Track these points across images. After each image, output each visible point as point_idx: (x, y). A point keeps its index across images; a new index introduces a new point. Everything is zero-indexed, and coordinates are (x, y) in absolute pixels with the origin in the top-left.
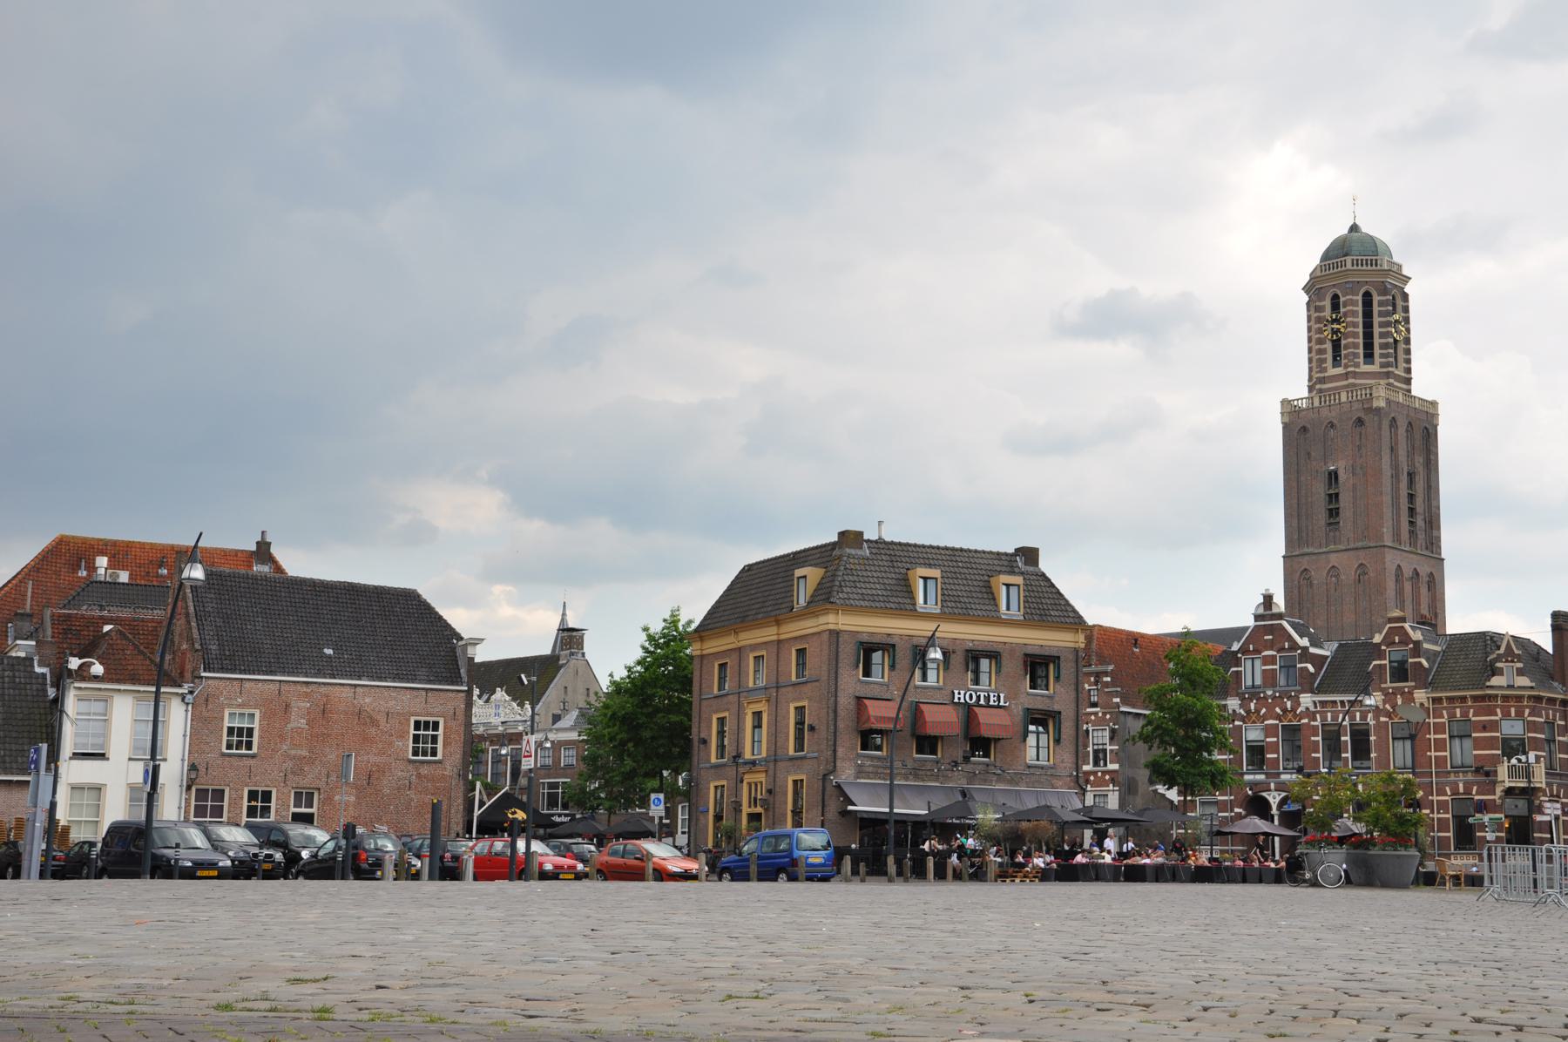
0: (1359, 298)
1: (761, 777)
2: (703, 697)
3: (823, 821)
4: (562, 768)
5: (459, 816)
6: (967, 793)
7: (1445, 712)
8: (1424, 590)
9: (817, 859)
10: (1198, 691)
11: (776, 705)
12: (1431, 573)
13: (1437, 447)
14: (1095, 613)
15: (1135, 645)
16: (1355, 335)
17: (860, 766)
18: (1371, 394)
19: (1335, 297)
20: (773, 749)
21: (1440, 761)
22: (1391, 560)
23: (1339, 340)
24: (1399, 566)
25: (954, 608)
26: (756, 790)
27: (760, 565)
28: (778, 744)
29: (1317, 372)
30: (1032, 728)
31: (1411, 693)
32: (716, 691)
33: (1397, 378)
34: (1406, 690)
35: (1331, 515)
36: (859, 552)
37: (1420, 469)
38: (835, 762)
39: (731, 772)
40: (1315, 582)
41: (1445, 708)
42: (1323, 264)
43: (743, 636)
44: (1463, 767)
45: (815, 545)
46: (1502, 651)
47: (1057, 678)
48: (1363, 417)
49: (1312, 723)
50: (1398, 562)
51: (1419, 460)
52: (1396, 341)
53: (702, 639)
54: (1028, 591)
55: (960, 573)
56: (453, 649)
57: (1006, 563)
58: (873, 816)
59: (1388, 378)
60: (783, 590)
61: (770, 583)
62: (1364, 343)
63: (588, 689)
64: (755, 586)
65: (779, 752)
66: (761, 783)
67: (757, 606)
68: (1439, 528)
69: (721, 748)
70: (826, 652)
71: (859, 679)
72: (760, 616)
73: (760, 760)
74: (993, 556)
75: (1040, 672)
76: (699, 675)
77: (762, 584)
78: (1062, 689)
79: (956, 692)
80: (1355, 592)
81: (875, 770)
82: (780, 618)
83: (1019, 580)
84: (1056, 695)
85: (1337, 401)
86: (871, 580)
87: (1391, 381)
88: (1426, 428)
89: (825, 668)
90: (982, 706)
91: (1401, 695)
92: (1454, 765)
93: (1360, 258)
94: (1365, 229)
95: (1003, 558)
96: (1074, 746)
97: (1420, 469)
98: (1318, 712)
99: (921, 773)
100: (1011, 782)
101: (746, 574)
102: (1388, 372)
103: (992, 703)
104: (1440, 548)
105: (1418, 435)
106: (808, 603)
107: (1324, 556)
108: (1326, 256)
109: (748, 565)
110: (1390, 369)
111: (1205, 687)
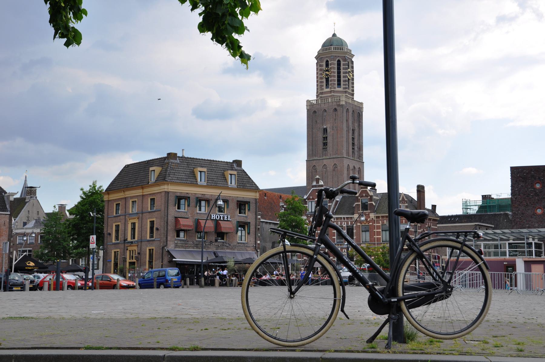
0: (336, 62)
2: (109, 217)
3: (162, 265)
4: (29, 244)
5: (6, 265)
6: (216, 253)
7: (380, 221)
9: (175, 279)
10: (297, 214)
11: (141, 220)
12: (359, 168)
15: (265, 196)
16: (334, 76)
17: (176, 243)
18: (340, 99)
19: (327, 61)
21: (378, 239)
22: (346, 162)
23: (328, 78)
24: (348, 165)
25: (212, 183)
26: (133, 253)
27: (133, 165)
28: (143, 235)
29: (320, 90)
30: (240, 229)
32: (115, 214)
33: (349, 93)
34: (367, 213)
35: (324, 145)
36: (175, 161)
37: (356, 128)
38: (167, 242)
40: (318, 170)
41: (380, 220)
42: (323, 48)
44: (386, 241)
47: (249, 210)
50: (348, 163)
51: (356, 125)
52: (349, 79)
53: (108, 194)
54: (238, 177)
55: (213, 170)
56: (3, 197)
57: (230, 166)
58: (182, 263)
59: (346, 93)
60: (144, 175)
61: (138, 172)
62: (337, 80)
63: (38, 212)
64: (131, 173)
65: (143, 238)
69: (117, 238)
70: (163, 200)
71: (176, 210)
72: (134, 185)
73: (135, 242)
74: (225, 163)
77: (134, 173)
79: (212, 215)
80: (333, 175)
81: (182, 245)
82: (143, 186)
83: (235, 173)
84: (249, 216)
85: (327, 102)
86: (180, 172)
87: (347, 94)
88: (359, 113)
89: (163, 206)
90: (221, 220)
92: (383, 240)
93: (336, 47)
94: (338, 35)
95: (229, 164)
96: (255, 236)
97: (356, 128)
98: (335, 222)
99: (199, 246)
100: (232, 249)
101: (126, 168)
102: (346, 91)
103: (225, 219)
105: (356, 115)
106: (156, 181)
107: (321, 161)
108: (324, 45)
109: (127, 165)
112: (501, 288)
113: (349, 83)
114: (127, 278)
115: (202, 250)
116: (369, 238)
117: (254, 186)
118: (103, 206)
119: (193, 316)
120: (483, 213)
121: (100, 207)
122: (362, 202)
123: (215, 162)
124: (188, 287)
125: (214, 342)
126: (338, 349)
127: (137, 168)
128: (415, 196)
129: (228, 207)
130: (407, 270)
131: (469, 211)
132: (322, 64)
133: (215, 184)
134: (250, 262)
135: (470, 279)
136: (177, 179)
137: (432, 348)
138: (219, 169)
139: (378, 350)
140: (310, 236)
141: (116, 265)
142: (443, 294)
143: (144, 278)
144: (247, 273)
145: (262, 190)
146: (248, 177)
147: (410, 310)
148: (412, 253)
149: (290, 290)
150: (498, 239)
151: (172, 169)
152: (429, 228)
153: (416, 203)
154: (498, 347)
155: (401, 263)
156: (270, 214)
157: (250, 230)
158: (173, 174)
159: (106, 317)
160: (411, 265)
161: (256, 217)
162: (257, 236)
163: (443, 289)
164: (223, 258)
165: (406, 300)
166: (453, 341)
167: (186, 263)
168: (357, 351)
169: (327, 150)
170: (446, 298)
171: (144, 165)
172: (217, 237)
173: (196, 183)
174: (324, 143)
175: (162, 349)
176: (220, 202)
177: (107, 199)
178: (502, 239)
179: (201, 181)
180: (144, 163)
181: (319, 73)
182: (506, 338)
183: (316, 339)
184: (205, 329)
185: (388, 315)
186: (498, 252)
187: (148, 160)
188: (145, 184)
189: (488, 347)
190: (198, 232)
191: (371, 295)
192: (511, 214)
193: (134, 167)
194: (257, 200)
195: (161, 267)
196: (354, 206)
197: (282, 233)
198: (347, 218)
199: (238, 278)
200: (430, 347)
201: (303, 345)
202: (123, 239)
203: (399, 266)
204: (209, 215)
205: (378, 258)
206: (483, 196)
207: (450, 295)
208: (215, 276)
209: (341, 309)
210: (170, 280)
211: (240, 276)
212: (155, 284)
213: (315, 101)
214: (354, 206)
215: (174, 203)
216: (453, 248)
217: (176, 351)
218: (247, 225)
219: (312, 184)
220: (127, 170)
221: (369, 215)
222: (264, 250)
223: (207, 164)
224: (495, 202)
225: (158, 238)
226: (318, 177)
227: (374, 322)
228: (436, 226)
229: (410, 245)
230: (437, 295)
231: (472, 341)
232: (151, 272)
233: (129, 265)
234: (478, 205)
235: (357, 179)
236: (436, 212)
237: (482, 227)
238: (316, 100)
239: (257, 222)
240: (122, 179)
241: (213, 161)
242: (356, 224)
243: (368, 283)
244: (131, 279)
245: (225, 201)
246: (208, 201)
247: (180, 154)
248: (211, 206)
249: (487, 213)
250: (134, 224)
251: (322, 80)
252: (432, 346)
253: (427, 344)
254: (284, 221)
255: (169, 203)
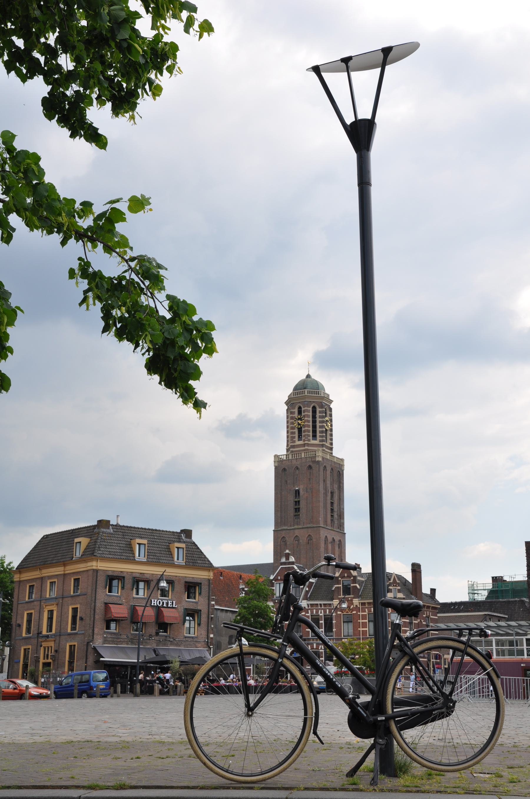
0: (311, 409)
1: (52, 644)
2: (19, 602)
6: (156, 650)
7: (366, 610)
8: (337, 548)
10: (261, 600)
13: (343, 480)
14: (217, 561)
15: (221, 575)
16: (309, 426)
17: (105, 637)
18: (315, 454)
19: (300, 408)
20: (59, 629)
23: (301, 428)
24: (326, 536)
27: (53, 535)
28: (62, 627)
29: (291, 443)
30: (187, 618)
31: (352, 600)
32: (27, 599)
33: (327, 447)
34: (350, 599)
35: (296, 511)
36: (108, 531)
37: (336, 490)
38: (93, 636)
39: (34, 641)
40: (288, 543)
41: (367, 608)
43: (44, 571)
45: (84, 526)
46: (391, 581)
47: (200, 594)
48: (312, 465)
49: (307, 614)
50: (326, 535)
51: (336, 486)
52: (326, 430)
53: (20, 573)
54: (187, 551)
55: (156, 542)
57: (177, 537)
59: (323, 447)
61: (59, 544)
62: (312, 430)
64: (50, 546)
65: (62, 631)
66: (51, 647)
67: (52, 556)
68: (343, 519)
69: (28, 631)
71: (107, 594)
72: (54, 561)
73: (51, 635)
74: (170, 533)
75: (192, 590)
76: (17, 591)
78: (202, 599)
79: (153, 600)
82: (66, 562)
83: (183, 545)
85: (300, 457)
87: (324, 448)
88: (339, 471)
90: (164, 607)
91: (347, 601)
93: (311, 390)
95: (176, 534)
96: (207, 627)
97: (336, 490)
99: (134, 641)
100: (177, 645)
101: (45, 540)
103: (169, 606)
104: (344, 528)
105: (335, 474)
106: (82, 555)
107: (292, 531)
108: (295, 389)
109: (46, 535)
110: (324, 443)
111: (264, 597)
112: (519, 698)
113: (326, 435)
114: (40, 684)
115: (139, 646)
116: (352, 631)
117: (207, 562)
118: (13, 589)
119: (122, 739)
120: (494, 600)
121: (8, 589)
122: (343, 584)
123: (158, 532)
124: (118, 696)
125: (147, 776)
126: (309, 785)
127: (58, 539)
128: (409, 577)
129: (173, 590)
130: (400, 673)
131: (476, 597)
132: (294, 410)
133: (158, 560)
134: (201, 661)
135: (479, 689)
136: (109, 553)
137: (430, 785)
138: (163, 541)
139: (361, 786)
140: (274, 634)
141: (25, 666)
142: (443, 710)
143: (61, 684)
144: (196, 676)
145: (217, 568)
146: (199, 551)
147: (402, 732)
148: (404, 656)
149: (248, 705)
150: (513, 634)
151: (103, 540)
152: (427, 619)
153: (411, 586)
154: (514, 782)
155: (390, 667)
156: (227, 598)
157: (200, 620)
158: (104, 546)
159: (6, 741)
160: (406, 667)
161: (209, 604)
162: (209, 628)
163: (443, 703)
164: (165, 657)
165: (396, 719)
166: (457, 774)
167: (117, 664)
168: (334, 788)
169: (299, 518)
170: (447, 716)
171: (67, 535)
172: (159, 628)
173: (132, 558)
174: (296, 509)
175: (77, 787)
176: (163, 584)
177: (18, 579)
178: (518, 634)
179: (139, 556)
180: (67, 533)
181: (289, 422)
182: (525, 769)
183: (281, 772)
184: (137, 757)
185: (373, 739)
186: (514, 650)
187: (72, 528)
188: (67, 559)
189: (502, 783)
190: (134, 623)
191: (351, 712)
192: (528, 601)
193: (54, 538)
194: (211, 582)
195: (84, 669)
196: (333, 589)
197: (239, 629)
198: (325, 605)
199: (184, 683)
200: (428, 782)
201: (264, 780)
202: (36, 632)
203: (387, 673)
204: (149, 600)
205: (363, 657)
206: (493, 578)
207: (452, 712)
208: (154, 681)
209: (313, 730)
210: (95, 687)
211: (187, 681)
212: (76, 692)
213: (285, 456)
214: (333, 589)
215: (104, 584)
216: (455, 650)
217: (96, 790)
218: (198, 613)
219: (280, 561)
220: (46, 542)
221: (352, 601)
222: (218, 648)
223: (148, 534)
224: (508, 586)
225: (82, 631)
226: (287, 551)
227: (357, 747)
228: (436, 616)
229: (401, 646)
230: (436, 712)
231: (481, 773)
232: (71, 676)
233: (43, 667)
234: (488, 590)
235: (333, 560)
236: (436, 598)
237: (494, 617)
238: (286, 455)
239: (210, 610)
240: (38, 553)
241: (156, 530)
242: (336, 613)
243: (348, 696)
244: (45, 686)
245: (170, 582)
246: (147, 582)
247: (113, 522)
248: (151, 588)
249: (498, 600)
250: (51, 612)
251: (294, 431)
252: (430, 781)
253: (424, 778)
254: (245, 608)
255: (98, 585)
